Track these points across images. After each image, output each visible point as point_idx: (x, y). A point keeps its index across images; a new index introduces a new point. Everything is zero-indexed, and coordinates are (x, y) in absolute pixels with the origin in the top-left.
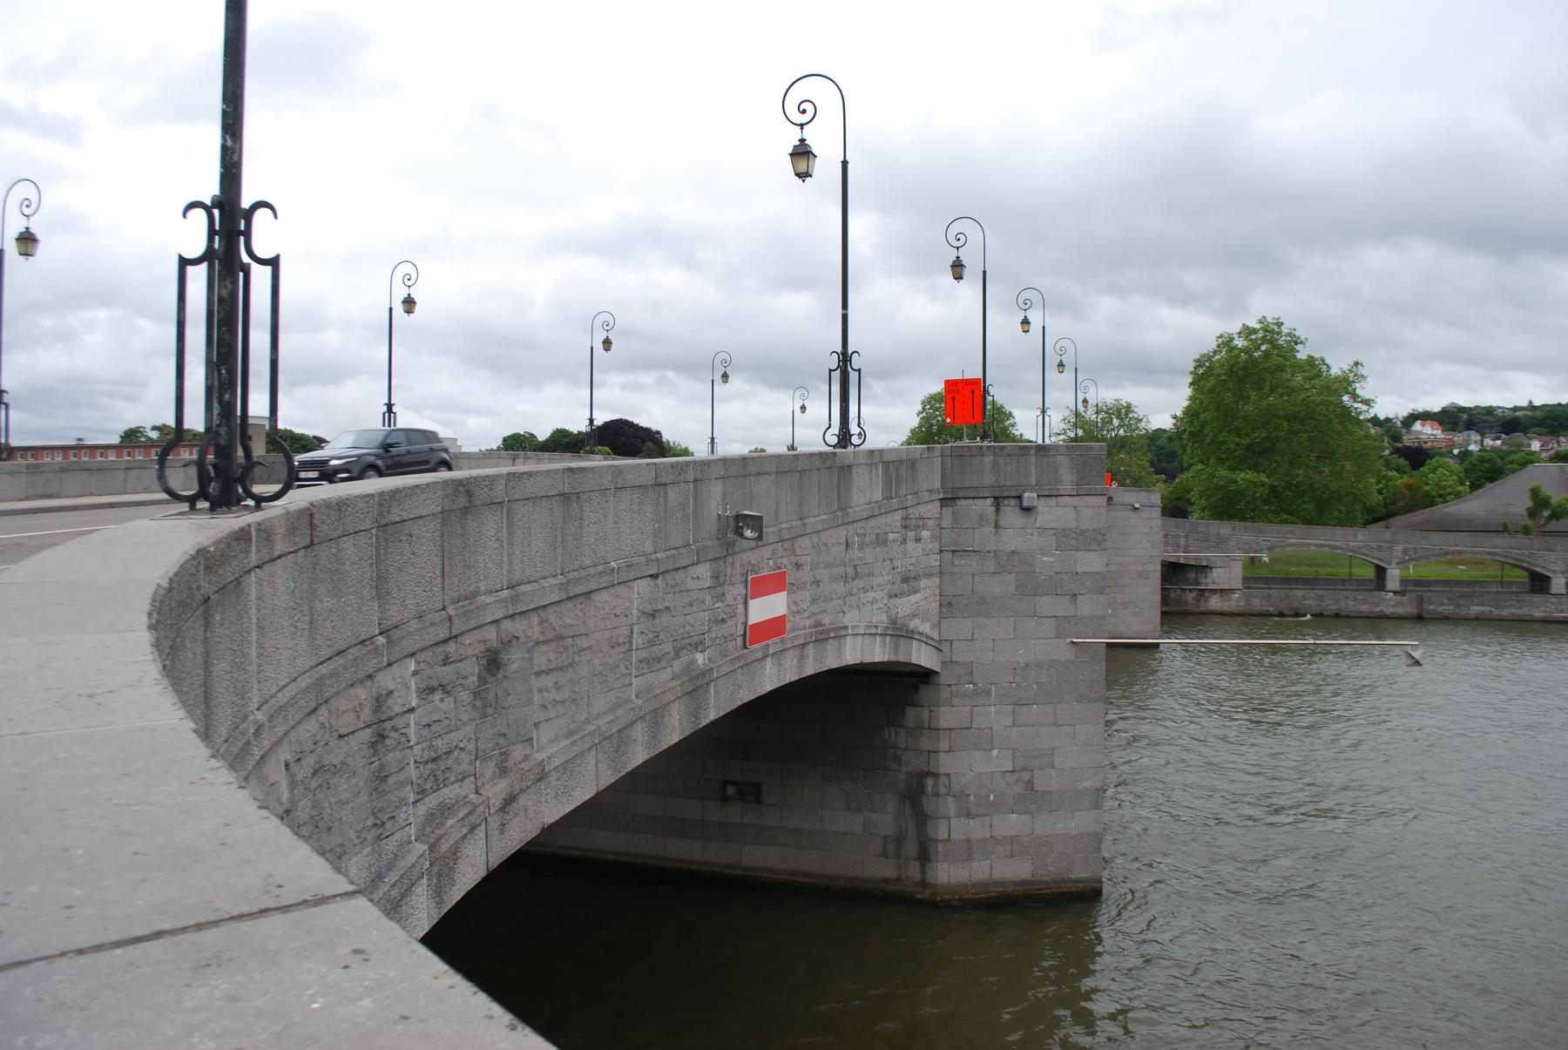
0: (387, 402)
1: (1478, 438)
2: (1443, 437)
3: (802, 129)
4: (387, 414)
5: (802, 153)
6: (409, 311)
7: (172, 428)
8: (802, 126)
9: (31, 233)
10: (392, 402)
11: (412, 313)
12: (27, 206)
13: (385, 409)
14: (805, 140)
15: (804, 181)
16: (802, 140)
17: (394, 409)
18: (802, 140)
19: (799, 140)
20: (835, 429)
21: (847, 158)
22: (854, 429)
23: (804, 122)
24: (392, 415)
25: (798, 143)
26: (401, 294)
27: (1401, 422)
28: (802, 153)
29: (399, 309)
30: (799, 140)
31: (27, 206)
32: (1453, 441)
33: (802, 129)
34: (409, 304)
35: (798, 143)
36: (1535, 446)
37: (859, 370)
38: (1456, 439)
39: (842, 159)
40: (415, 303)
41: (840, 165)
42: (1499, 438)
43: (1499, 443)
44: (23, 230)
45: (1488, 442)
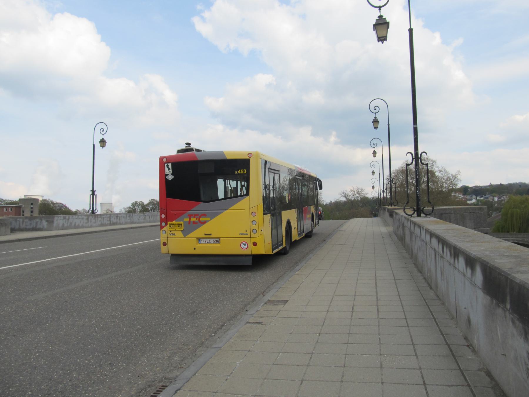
0: (92, 190)
1: (475, 197)
2: (463, 197)
3: (375, 114)
4: (92, 196)
5: (376, 121)
6: (103, 146)
7: (157, 201)
8: (375, 113)
9: (104, 140)
10: (95, 190)
11: (105, 147)
12: (103, 131)
13: (91, 193)
14: (376, 118)
15: (376, 129)
16: (375, 118)
17: (95, 193)
18: (375, 118)
19: (375, 118)
20: (91, 209)
21: (389, 123)
22: (94, 210)
23: (104, 134)
24: (94, 196)
25: (374, 118)
26: (99, 138)
27: (131, 205)
28: (376, 121)
29: (97, 145)
30: (375, 118)
31: (103, 131)
32: (466, 198)
33: (375, 114)
34: (103, 143)
35: (374, 118)
36: (496, 199)
37: (96, 195)
38: (467, 197)
39: (388, 123)
40: (106, 142)
41: (387, 125)
42: (482, 197)
43: (482, 198)
44: (102, 139)
45: (479, 198)
